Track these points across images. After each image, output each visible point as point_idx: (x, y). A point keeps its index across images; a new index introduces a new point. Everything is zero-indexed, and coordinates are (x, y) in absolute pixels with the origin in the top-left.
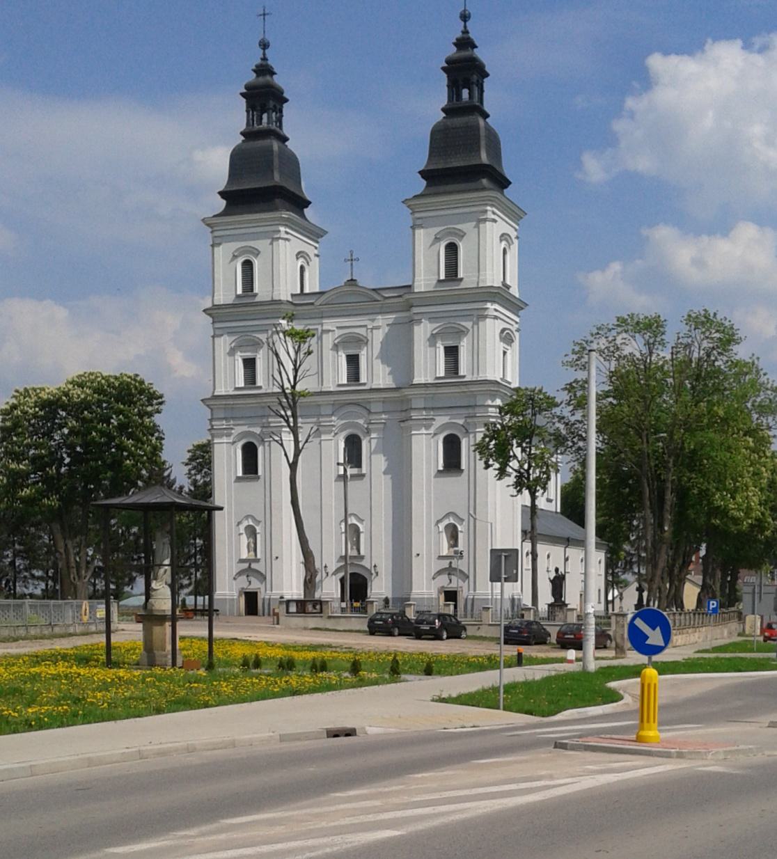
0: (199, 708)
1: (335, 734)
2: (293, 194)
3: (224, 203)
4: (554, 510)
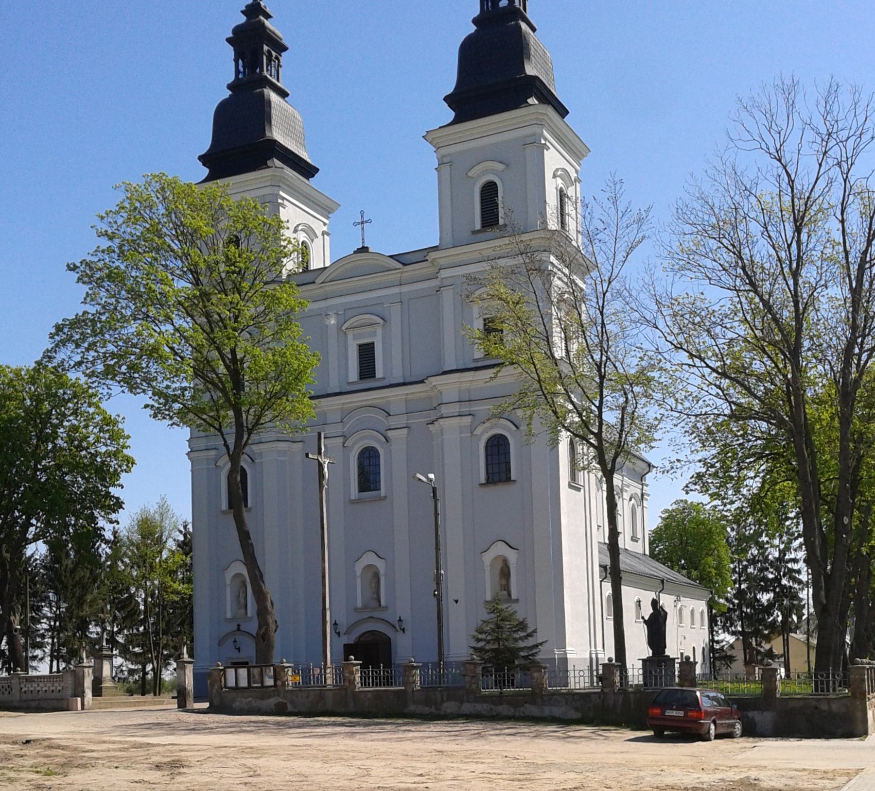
4: (641, 552)
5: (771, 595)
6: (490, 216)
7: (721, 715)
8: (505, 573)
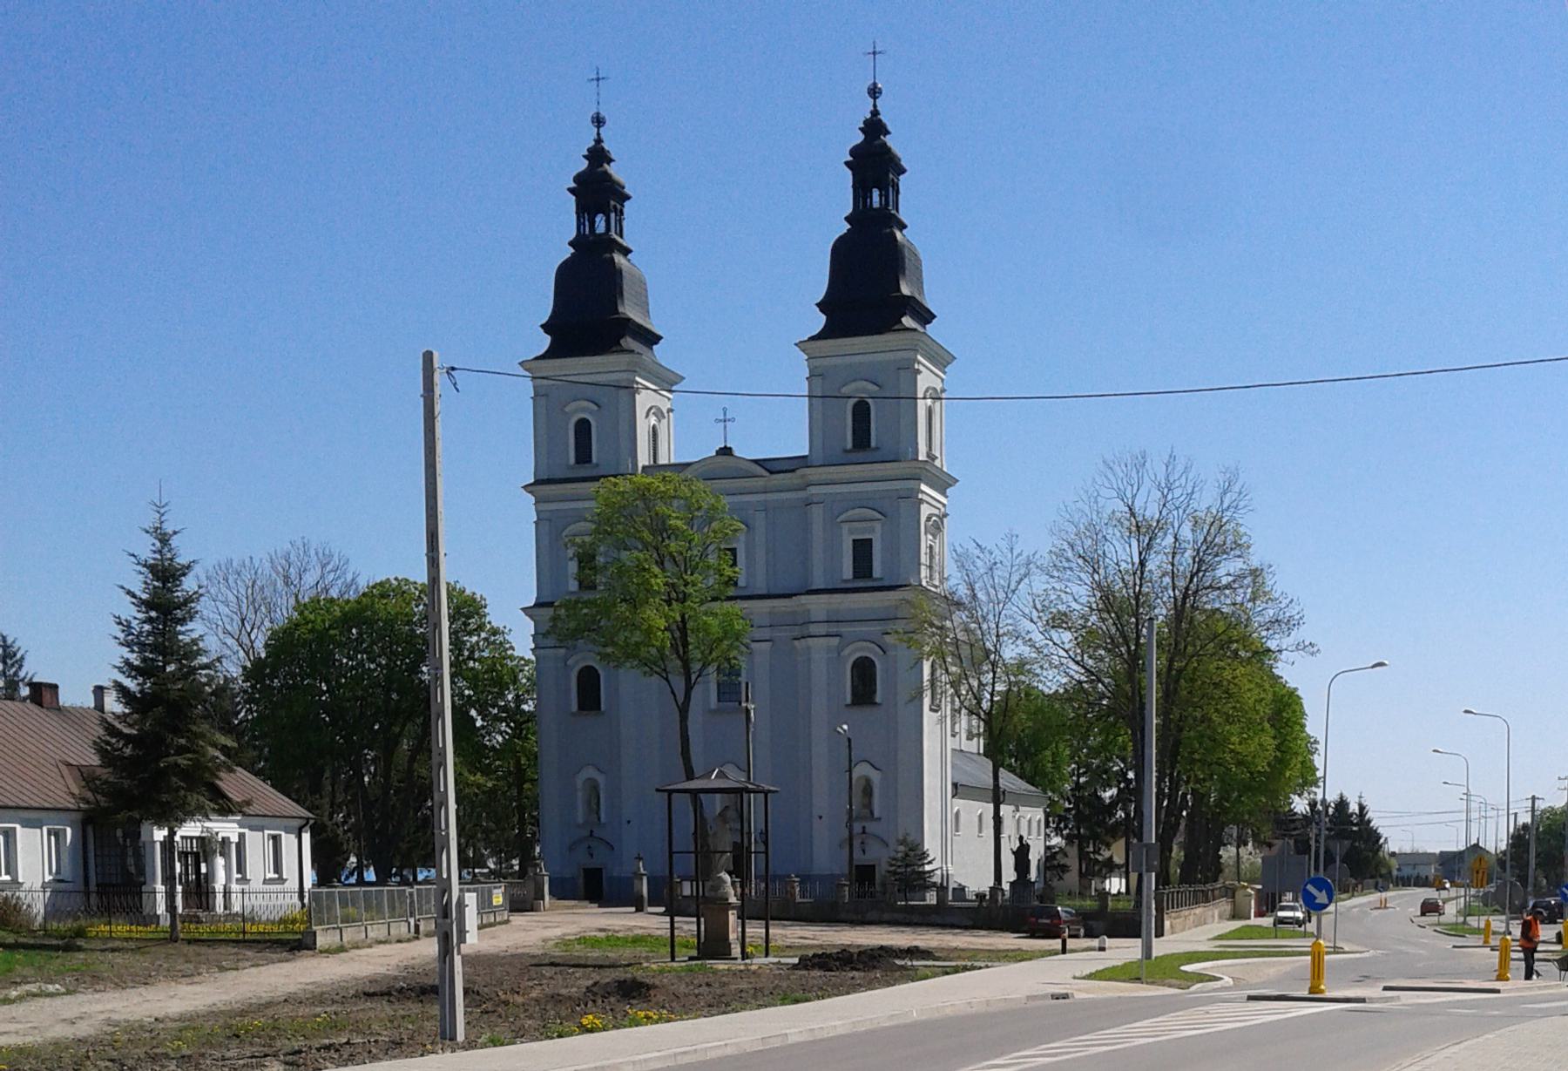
0: (374, 1058)
1: (1056, 997)
2: (640, 326)
3: (547, 340)
5: (1114, 791)
6: (862, 438)
7: (1072, 922)
8: (868, 791)
